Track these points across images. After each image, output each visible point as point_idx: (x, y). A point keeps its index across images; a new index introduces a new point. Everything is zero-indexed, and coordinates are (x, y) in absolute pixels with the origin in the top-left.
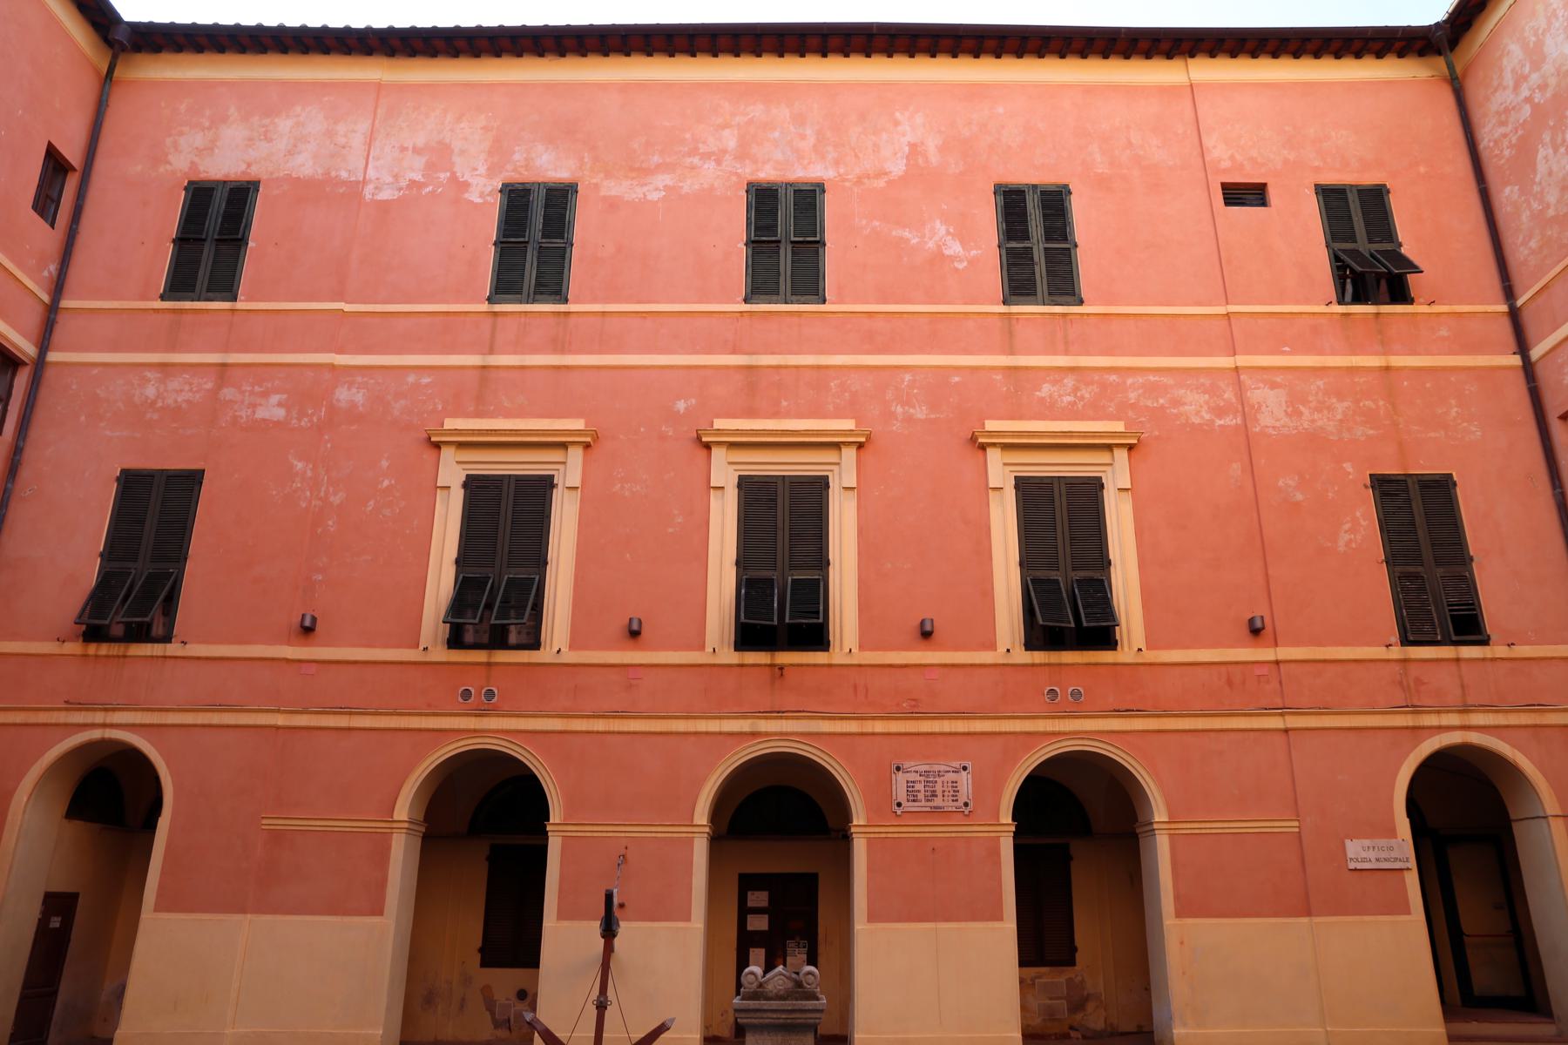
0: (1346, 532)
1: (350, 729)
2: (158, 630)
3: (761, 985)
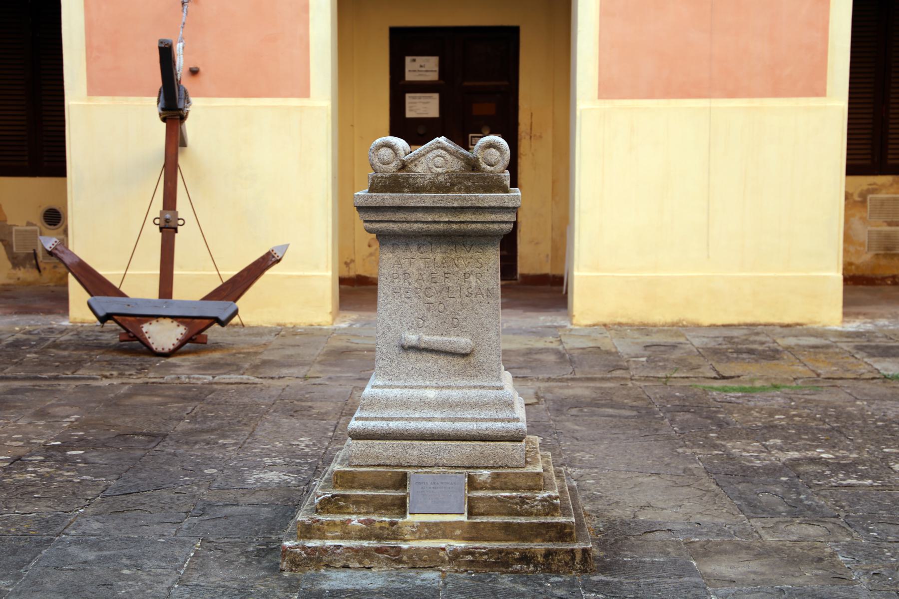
3: (404, 166)
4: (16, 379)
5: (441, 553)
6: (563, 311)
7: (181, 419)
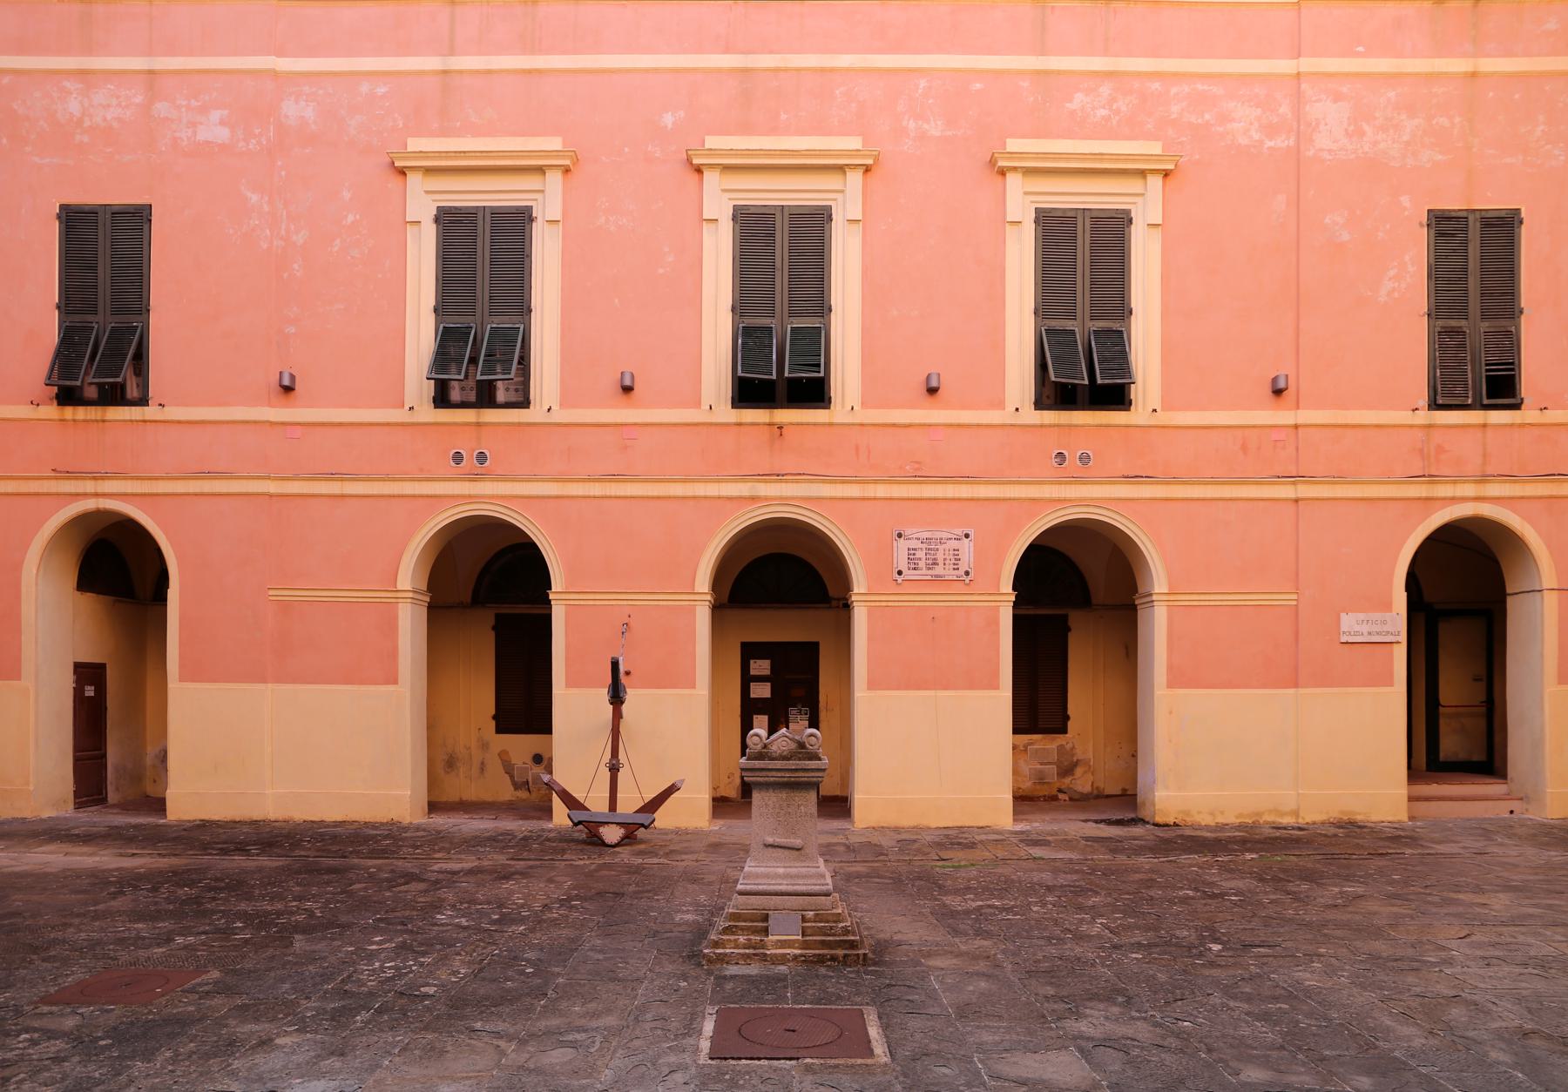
0: (1390, 279)
1: (343, 496)
2: (132, 392)
3: (765, 746)
4: (529, 860)
5: (788, 956)
6: (849, 819)
7: (630, 885)
